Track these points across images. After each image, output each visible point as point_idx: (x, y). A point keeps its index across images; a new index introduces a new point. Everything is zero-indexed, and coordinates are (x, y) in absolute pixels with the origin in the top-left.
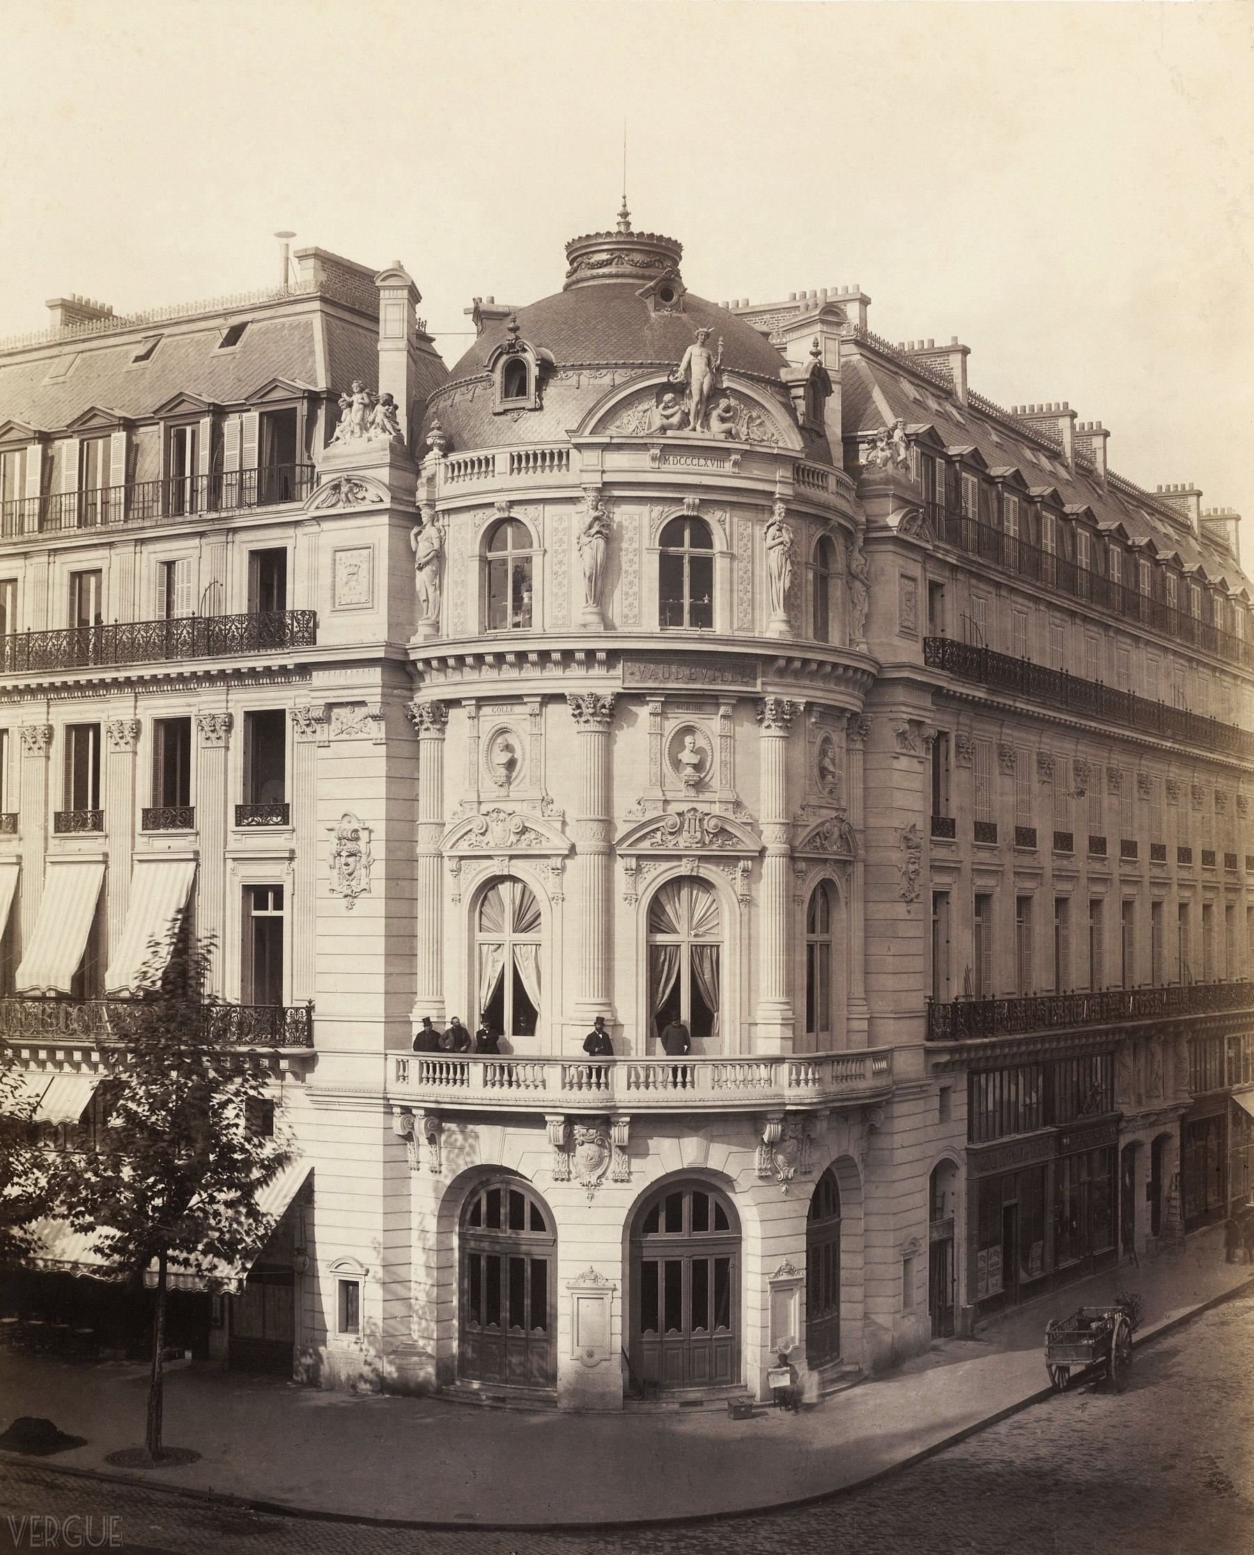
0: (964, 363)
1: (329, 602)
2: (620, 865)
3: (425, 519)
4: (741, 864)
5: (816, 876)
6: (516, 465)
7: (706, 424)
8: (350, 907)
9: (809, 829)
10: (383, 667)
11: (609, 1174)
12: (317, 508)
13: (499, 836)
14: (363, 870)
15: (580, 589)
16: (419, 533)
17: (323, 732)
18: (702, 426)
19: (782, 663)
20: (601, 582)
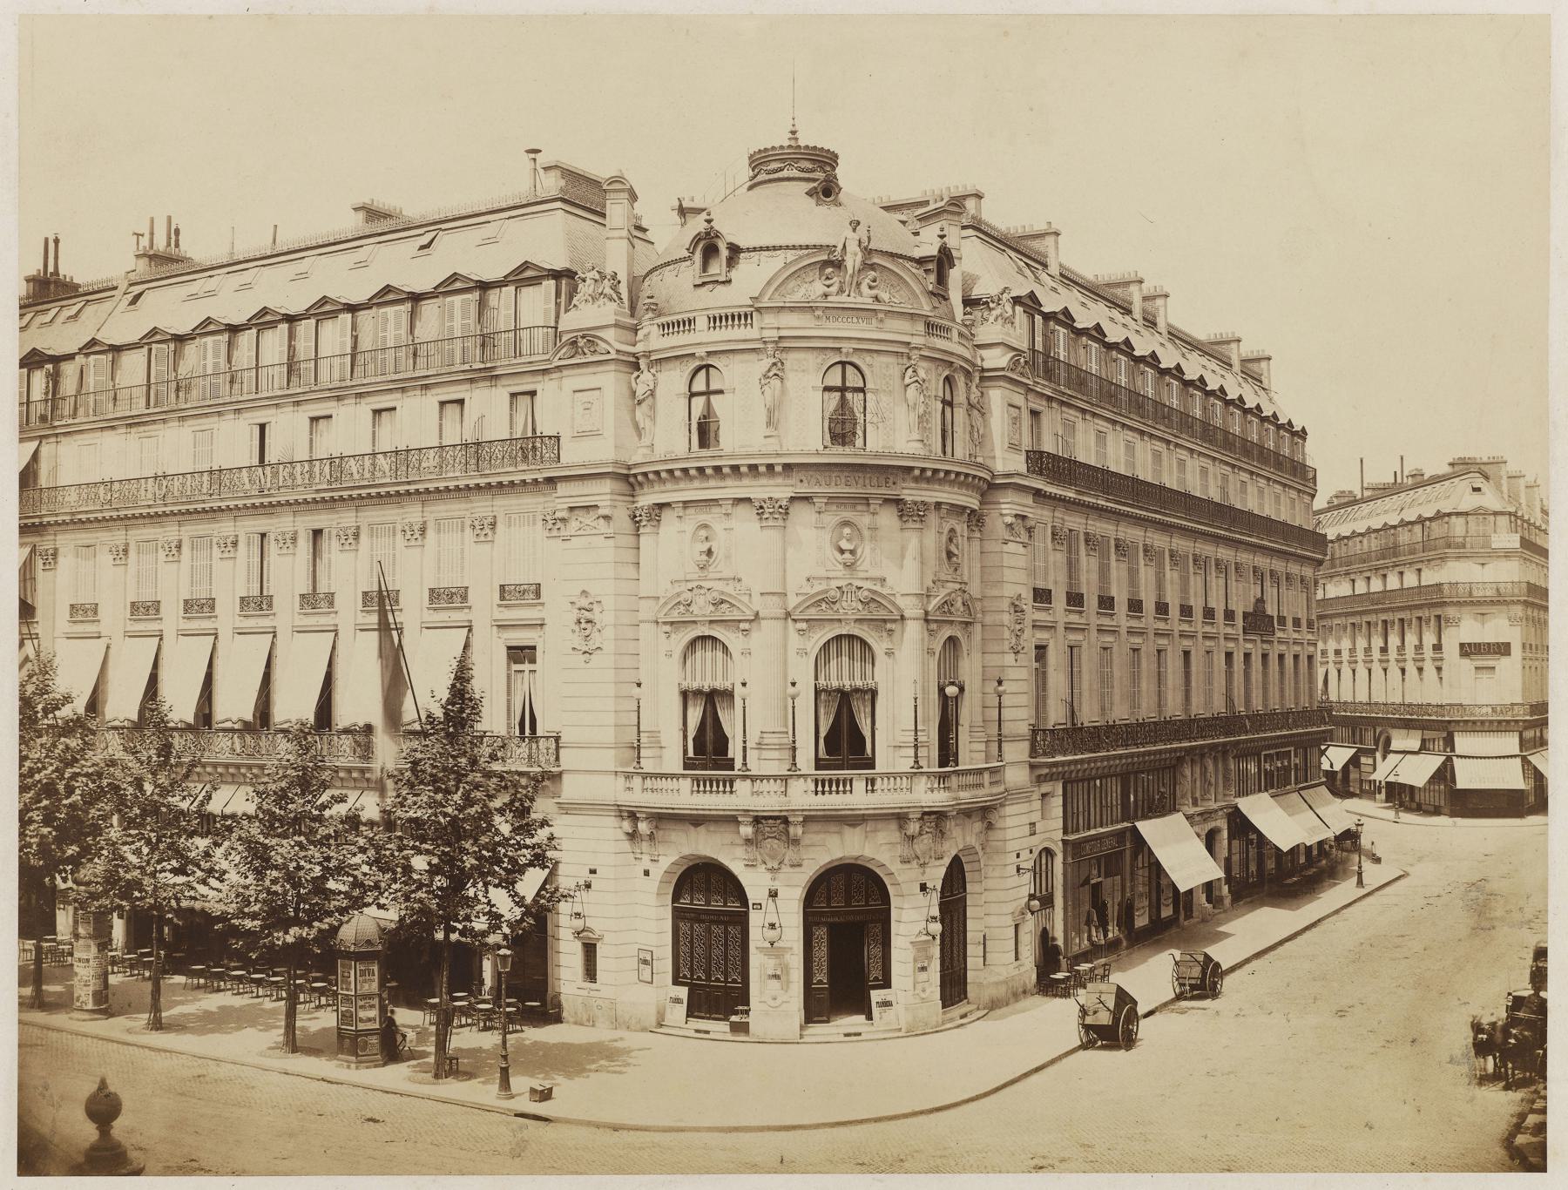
13: (702, 607)
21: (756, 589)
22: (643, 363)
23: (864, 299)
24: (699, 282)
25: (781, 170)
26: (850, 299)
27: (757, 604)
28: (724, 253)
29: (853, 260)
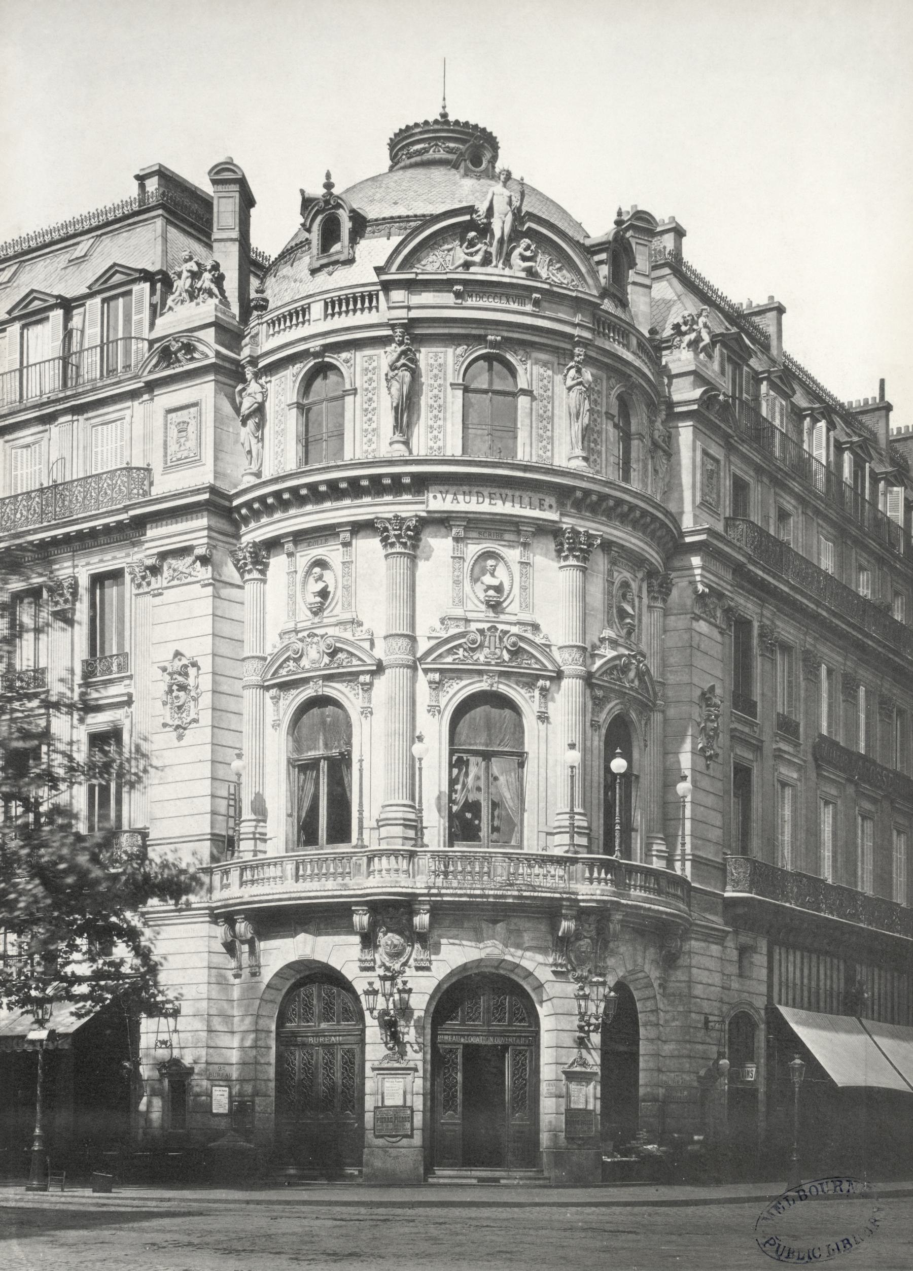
0: (779, 324)
1: (161, 459)
2: (422, 681)
3: (249, 376)
4: (541, 683)
5: (612, 707)
6: (330, 311)
7: (507, 263)
8: (180, 738)
9: (605, 659)
10: (207, 510)
11: (411, 962)
12: (150, 372)
13: (314, 657)
14: (192, 703)
15: (387, 420)
16: (244, 389)
17: (157, 583)
18: (504, 264)
19: (579, 494)
20: (406, 411)
21: (380, 632)
22: (249, 372)
23: (515, 272)
24: (317, 265)
25: (426, 150)
26: (496, 271)
27: (380, 652)
28: (346, 225)
29: (501, 225)
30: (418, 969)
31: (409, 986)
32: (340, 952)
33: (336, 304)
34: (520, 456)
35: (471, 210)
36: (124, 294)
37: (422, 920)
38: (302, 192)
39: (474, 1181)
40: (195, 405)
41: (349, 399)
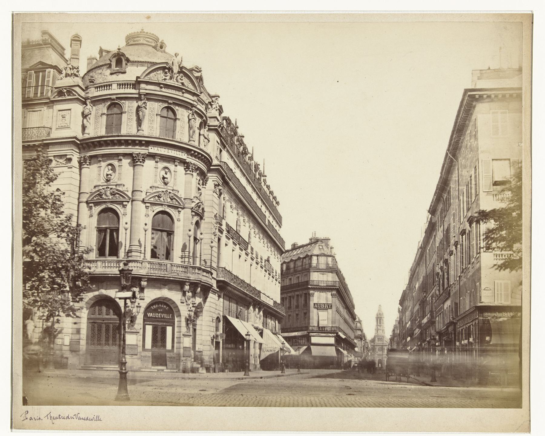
19: (193, 152)
30: (140, 299)
31: (140, 305)
32: (175, 296)
33: (121, 85)
34: (124, 132)
35: (167, 63)
36: (42, 71)
37: (144, 283)
38: (100, 47)
39: (95, 369)
40: (70, 110)
41: (123, 115)
